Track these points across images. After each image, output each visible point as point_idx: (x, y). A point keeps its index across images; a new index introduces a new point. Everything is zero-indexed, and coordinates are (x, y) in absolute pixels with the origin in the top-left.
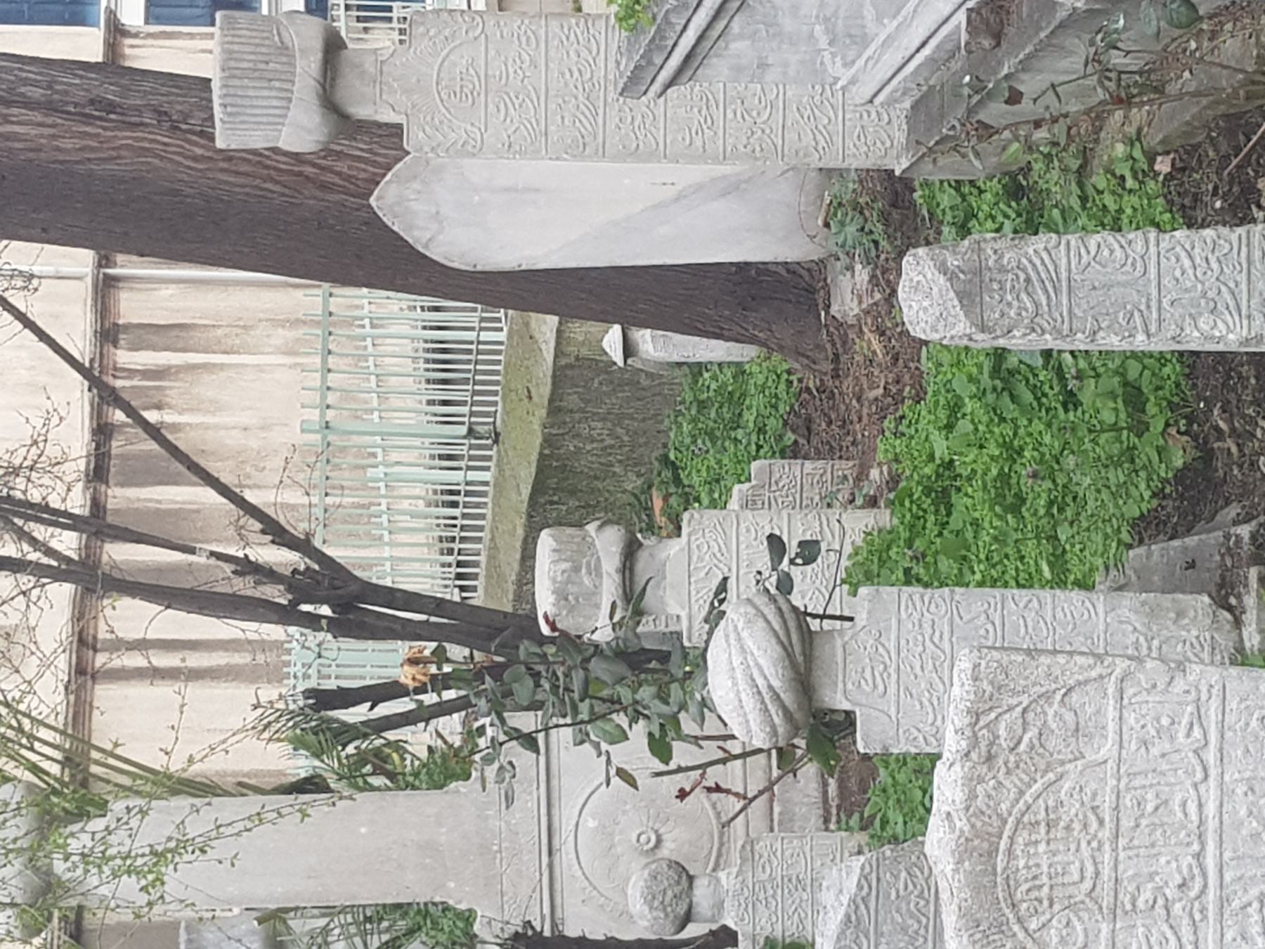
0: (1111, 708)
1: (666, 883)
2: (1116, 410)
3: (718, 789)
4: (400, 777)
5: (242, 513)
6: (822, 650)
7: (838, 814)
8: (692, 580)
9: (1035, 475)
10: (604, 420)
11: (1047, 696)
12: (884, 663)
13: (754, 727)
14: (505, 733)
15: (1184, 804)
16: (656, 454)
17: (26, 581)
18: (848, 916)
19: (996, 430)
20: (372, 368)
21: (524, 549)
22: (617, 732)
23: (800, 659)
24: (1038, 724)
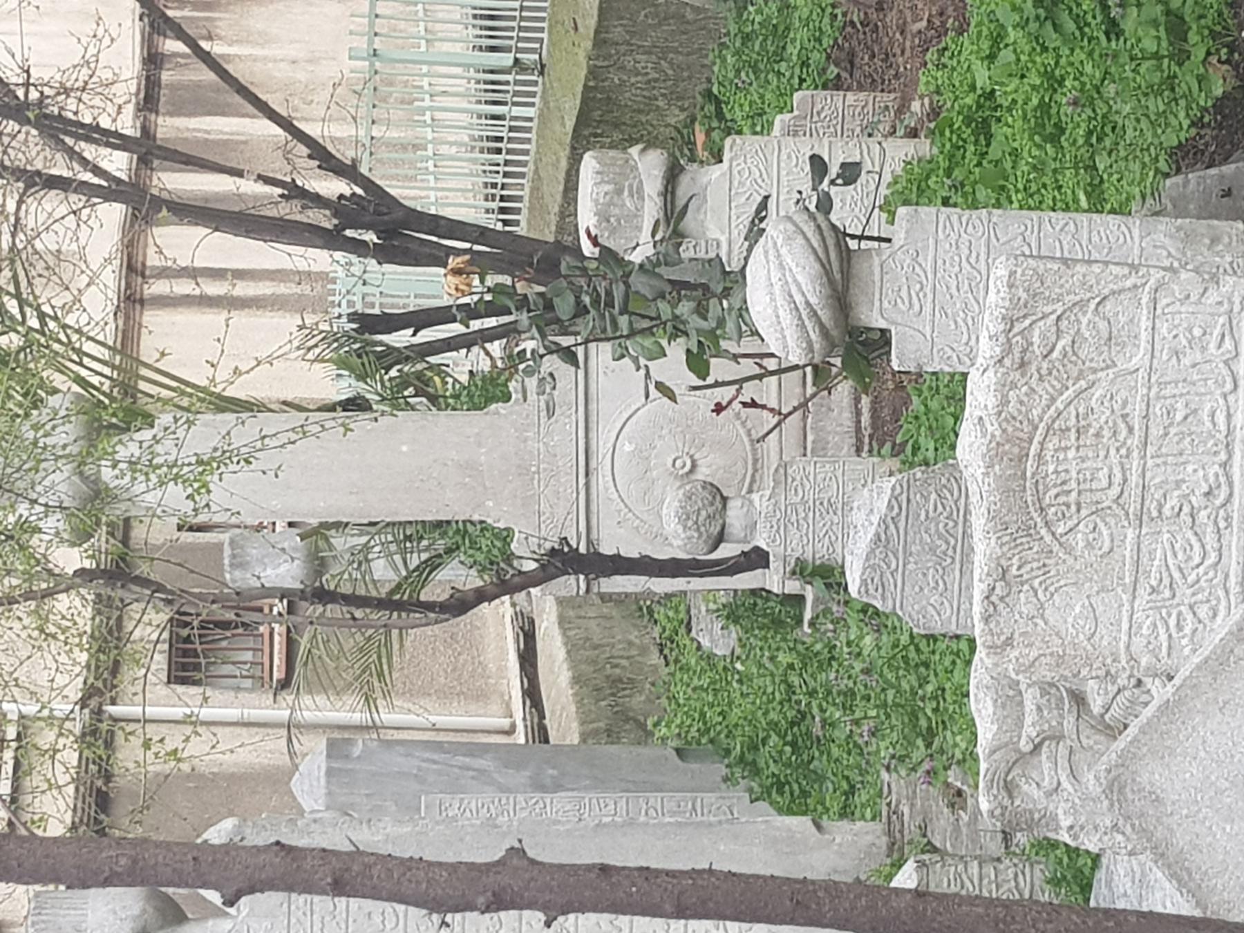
0: (1144, 318)
1: (700, 504)
2: (1158, 38)
3: (753, 404)
4: (441, 400)
5: (290, 138)
6: (859, 267)
7: (870, 444)
8: (733, 205)
9: (1075, 103)
10: (650, 53)
11: (1082, 304)
12: (921, 283)
13: (791, 343)
14: (545, 347)
15: (1213, 415)
16: (699, 88)
17: (77, 200)
18: (878, 535)
19: (1038, 59)
20: (423, 33)
21: (567, 181)
22: (655, 348)
23: (838, 276)
24: (1072, 332)
